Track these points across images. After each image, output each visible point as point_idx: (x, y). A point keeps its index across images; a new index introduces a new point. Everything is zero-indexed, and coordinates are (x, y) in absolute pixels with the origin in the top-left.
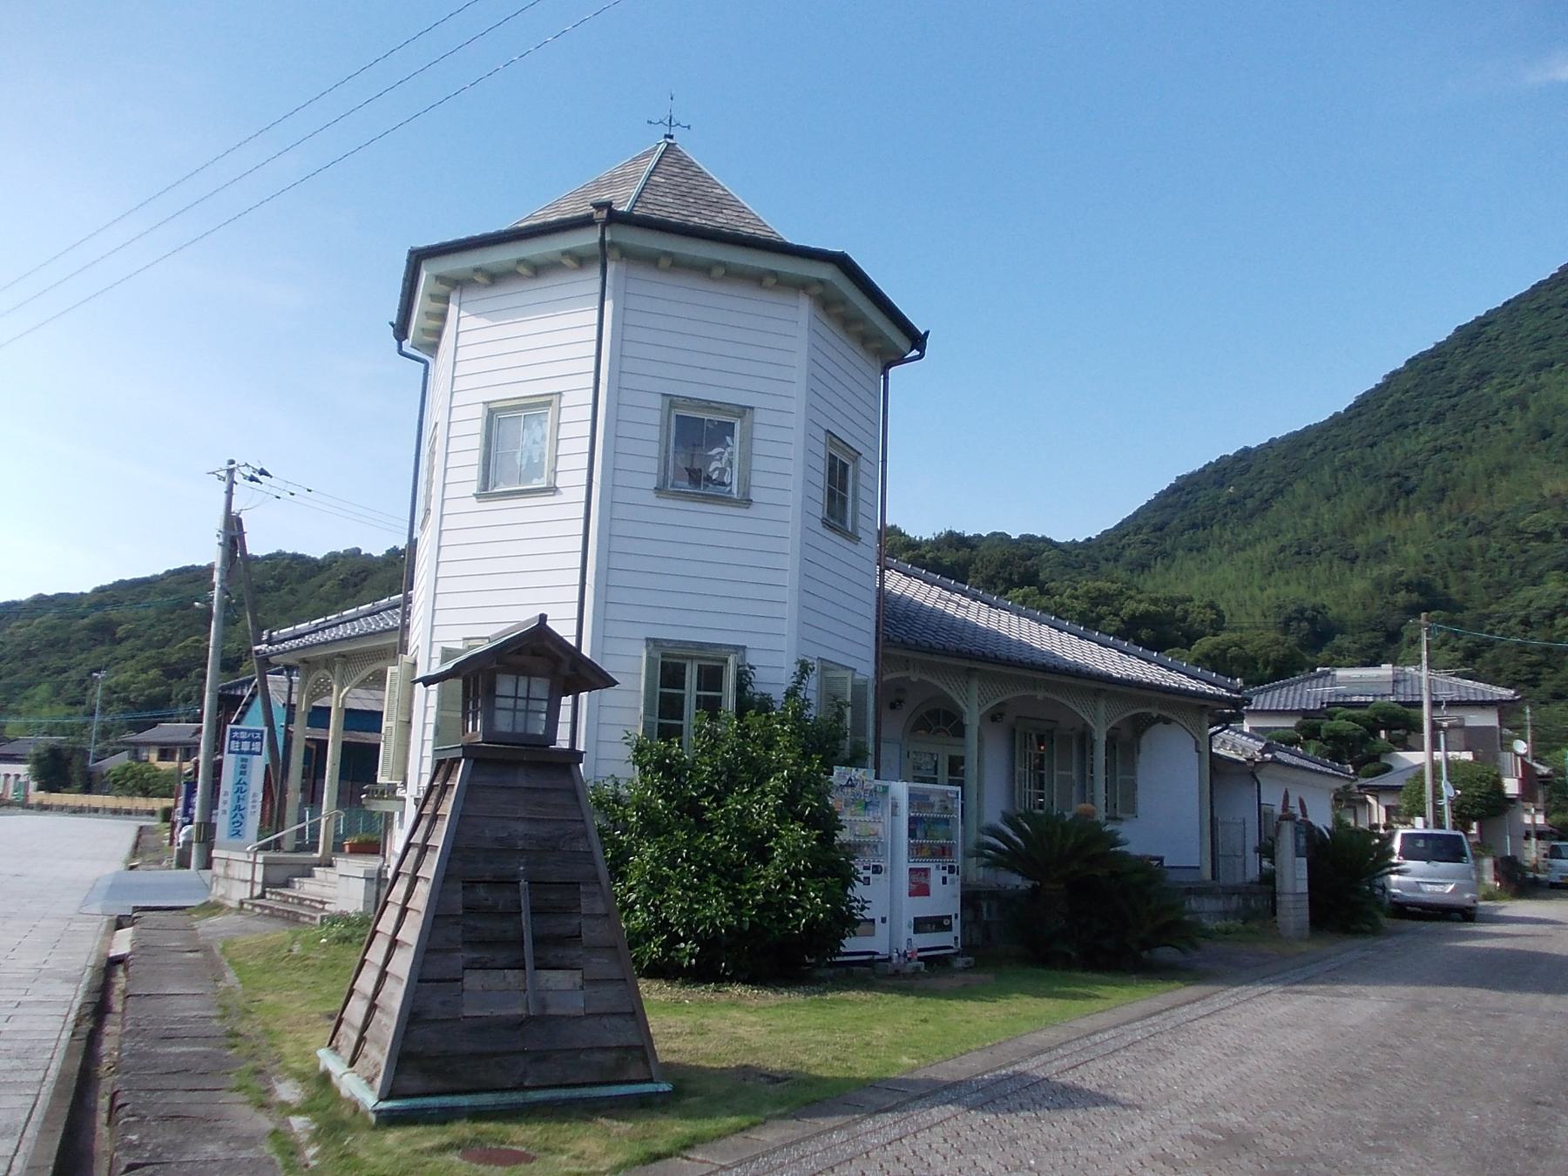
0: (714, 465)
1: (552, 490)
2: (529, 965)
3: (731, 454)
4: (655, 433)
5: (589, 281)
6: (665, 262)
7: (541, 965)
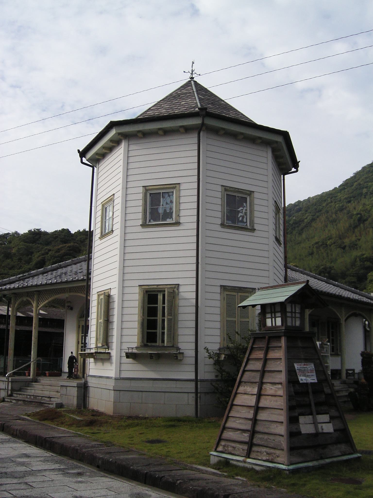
0: (240, 214)
1: (178, 223)
2: (314, 413)
3: (246, 210)
4: (219, 201)
5: (192, 139)
6: (222, 132)
7: (318, 413)
